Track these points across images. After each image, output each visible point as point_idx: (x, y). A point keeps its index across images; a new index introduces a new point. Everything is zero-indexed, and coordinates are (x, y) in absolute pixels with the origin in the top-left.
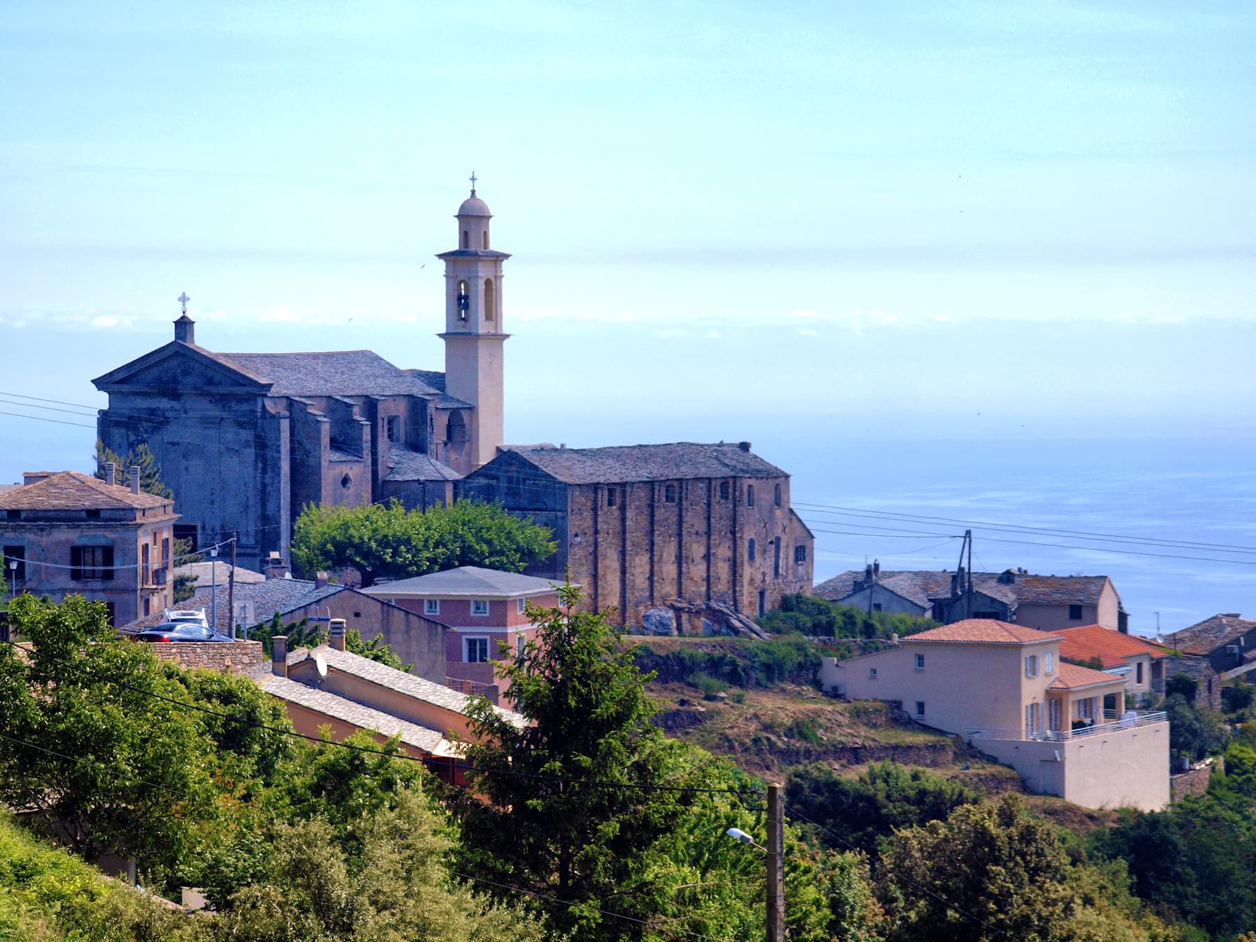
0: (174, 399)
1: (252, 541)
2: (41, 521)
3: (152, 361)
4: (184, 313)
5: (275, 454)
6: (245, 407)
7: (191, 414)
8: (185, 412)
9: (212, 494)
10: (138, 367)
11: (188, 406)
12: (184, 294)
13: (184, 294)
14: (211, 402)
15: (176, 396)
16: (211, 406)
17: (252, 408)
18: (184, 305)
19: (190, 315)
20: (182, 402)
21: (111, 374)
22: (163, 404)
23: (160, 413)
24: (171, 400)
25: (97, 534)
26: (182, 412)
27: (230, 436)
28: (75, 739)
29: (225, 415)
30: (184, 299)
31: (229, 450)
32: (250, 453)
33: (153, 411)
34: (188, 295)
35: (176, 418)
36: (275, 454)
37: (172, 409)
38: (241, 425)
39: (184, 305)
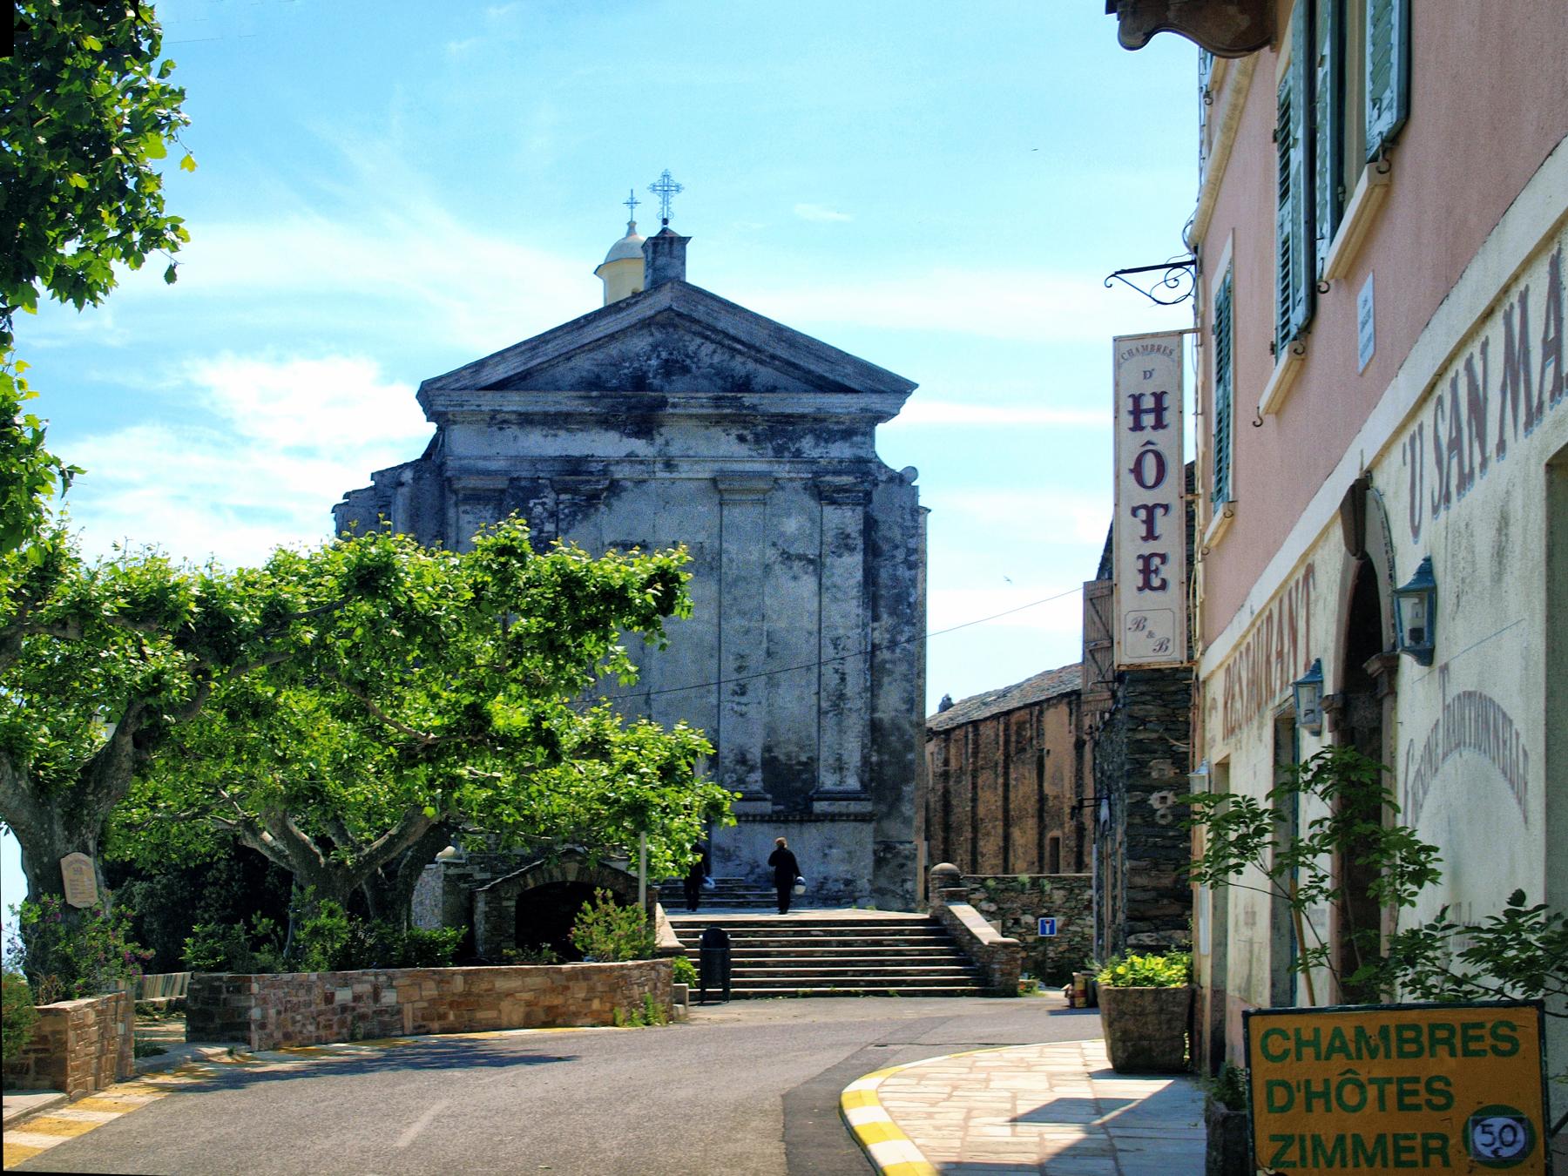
0: (637, 434)
1: (853, 783)
2: (383, 846)
3: (725, 323)
4: (665, 221)
5: (903, 572)
6: (840, 451)
7: (685, 470)
8: (669, 465)
9: (740, 669)
10: (551, 349)
11: (674, 450)
12: (666, 176)
13: (666, 176)
14: (741, 439)
15: (644, 423)
16: (742, 450)
17: (862, 453)
18: (666, 202)
19: (677, 228)
20: (659, 441)
21: (480, 365)
22: (606, 445)
23: (595, 467)
24: (629, 436)
25: (712, 1017)
26: (659, 466)
27: (791, 525)
28: (16, 171)
29: (783, 470)
30: (666, 188)
31: (787, 557)
32: (849, 567)
33: (575, 465)
34: (676, 178)
35: (640, 483)
36: (903, 572)
37: (631, 458)
38: (823, 494)
39: (666, 202)
